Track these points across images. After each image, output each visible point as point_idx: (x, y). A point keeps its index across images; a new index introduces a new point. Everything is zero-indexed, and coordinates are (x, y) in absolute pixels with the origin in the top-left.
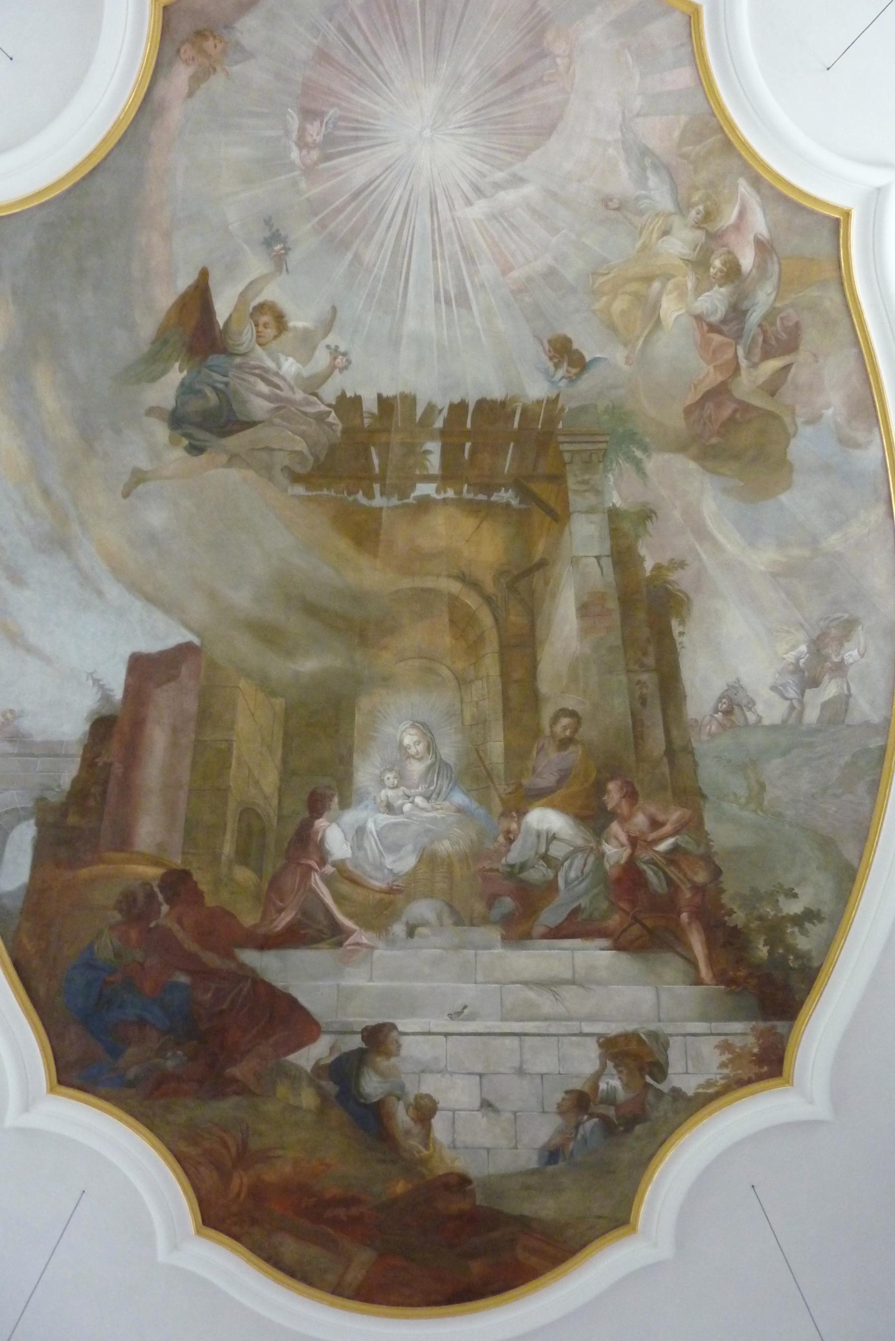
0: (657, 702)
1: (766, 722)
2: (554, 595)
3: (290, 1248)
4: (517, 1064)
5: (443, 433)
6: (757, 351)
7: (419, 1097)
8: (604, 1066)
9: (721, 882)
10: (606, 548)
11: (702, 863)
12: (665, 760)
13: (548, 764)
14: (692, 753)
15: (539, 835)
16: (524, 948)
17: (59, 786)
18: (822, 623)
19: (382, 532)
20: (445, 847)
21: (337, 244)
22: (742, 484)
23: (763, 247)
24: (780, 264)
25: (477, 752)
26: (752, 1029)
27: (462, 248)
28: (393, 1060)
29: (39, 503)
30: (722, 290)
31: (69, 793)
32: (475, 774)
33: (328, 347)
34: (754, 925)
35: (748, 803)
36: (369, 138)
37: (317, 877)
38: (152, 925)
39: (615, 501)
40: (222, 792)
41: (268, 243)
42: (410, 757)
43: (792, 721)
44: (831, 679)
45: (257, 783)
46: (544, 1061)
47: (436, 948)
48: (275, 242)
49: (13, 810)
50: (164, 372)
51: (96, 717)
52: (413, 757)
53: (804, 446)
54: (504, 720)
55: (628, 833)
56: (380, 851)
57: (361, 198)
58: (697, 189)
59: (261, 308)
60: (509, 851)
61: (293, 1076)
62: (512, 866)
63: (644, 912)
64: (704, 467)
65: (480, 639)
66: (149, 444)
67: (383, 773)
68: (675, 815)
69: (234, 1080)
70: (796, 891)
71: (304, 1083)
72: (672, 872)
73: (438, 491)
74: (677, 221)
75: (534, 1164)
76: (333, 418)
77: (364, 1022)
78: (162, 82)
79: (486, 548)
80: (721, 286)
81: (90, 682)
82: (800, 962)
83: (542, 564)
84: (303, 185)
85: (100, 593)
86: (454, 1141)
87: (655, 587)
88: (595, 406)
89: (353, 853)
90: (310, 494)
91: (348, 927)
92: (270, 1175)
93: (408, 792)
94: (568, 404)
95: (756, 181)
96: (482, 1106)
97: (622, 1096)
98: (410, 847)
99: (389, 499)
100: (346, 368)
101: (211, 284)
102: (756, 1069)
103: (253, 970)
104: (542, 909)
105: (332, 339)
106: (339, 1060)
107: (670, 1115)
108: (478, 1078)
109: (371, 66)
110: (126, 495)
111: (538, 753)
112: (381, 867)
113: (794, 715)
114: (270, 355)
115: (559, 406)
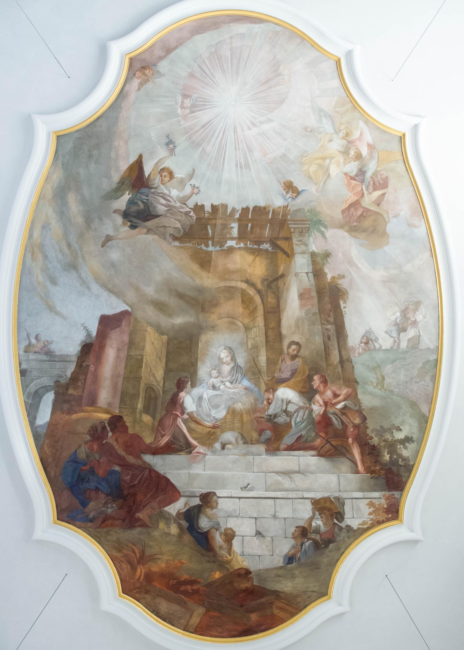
0: (335, 339)
1: (384, 348)
2: (288, 290)
3: (164, 606)
4: (273, 513)
5: (239, 220)
6: (371, 188)
7: (226, 529)
8: (314, 514)
9: (367, 423)
10: (310, 269)
11: (357, 414)
12: (339, 365)
13: (287, 367)
14: (351, 362)
15: (282, 401)
16: (276, 455)
17: (66, 376)
18: (406, 303)
19: (212, 261)
20: (239, 406)
21: (196, 145)
22: (367, 242)
23: (371, 147)
24: (378, 153)
25: (254, 360)
26: (384, 496)
27: (247, 146)
28: (214, 510)
29: (66, 250)
30: (355, 163)
31: (70, 378)
32: (253, 372)
33: (191, 185)
34: (383, 444)
35: (377, 385)
36: (210, 105)
37: (180, 420)
38: (104, 442)
39: (313, 249)
40: (138, 379)
41: (167, 144)
42: (223, 363)
43: (395, 347)
44: (411, 328)
45: (154, 375)
46: (285, 511)
47: (234, 455)
48: (170, 144)
49: (45, 386)
50: (122, 195)
51: (84, 344)
52: (225, 363)
53: (393, 227)
54: (266, 346)
55: (323, 399)
56: (210, 409)
57: (205, 128)
58: (343, 124)
59: (163, 170)
60: (269, 408)
61: (167, 518)
62: (270, 416)
63: (333, 437)
64: (351, 235)
65: (255, 309)
66: (114, 225)
67: (211, 371)
68: (344, 391)
69: (139, 519)
70: (401, 427)
71: (172, 521)
72: (344, 418)
73: (237, 244)
74: (335, 136)
75: (281, 564)
76: (192, 214)
77: (201, 491)
78: (128, 85)
79: (258, 269)
80: (354, 161)
81: (82, 328)
82: (404, 462)
83: (283, 276)
84: (182, 122)
85: (89, 288)
86: (243, 552)
87: (333, 286)
88: (304, 210)
89: (197, 409)
90: (181, 245)
91: (194, 444)
92: (155, 569)
93: (222, 380)
94: (292, 208)
95: (367, 122)
96: (256, 534)
97: (323, 529)
98: (223, 406)
99: (215, 247)
100: (198, 193)
101: (143, 160)
102: (386, 516)
103: (149, 465)
104: (285, 436)
105: (193, 182)
106: (188, 510)
107: (346, 538)
108: (254, 520)
109: (210, 79)
110: (103, 246)
111: (282, 362)
112: (209, 416)
113: (396, 344)
114: (166, 188)
115: (288, 209)
